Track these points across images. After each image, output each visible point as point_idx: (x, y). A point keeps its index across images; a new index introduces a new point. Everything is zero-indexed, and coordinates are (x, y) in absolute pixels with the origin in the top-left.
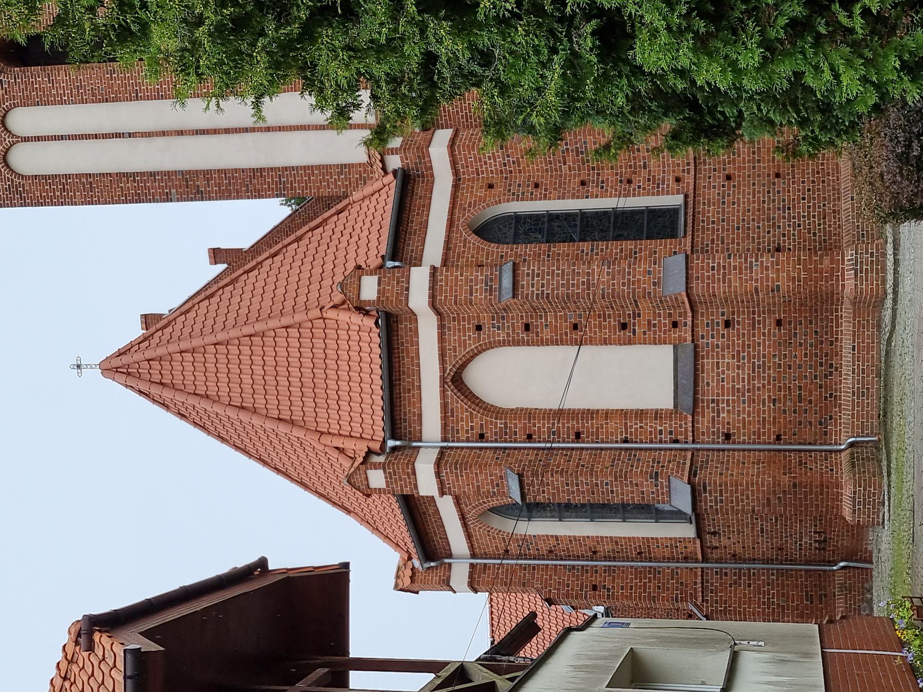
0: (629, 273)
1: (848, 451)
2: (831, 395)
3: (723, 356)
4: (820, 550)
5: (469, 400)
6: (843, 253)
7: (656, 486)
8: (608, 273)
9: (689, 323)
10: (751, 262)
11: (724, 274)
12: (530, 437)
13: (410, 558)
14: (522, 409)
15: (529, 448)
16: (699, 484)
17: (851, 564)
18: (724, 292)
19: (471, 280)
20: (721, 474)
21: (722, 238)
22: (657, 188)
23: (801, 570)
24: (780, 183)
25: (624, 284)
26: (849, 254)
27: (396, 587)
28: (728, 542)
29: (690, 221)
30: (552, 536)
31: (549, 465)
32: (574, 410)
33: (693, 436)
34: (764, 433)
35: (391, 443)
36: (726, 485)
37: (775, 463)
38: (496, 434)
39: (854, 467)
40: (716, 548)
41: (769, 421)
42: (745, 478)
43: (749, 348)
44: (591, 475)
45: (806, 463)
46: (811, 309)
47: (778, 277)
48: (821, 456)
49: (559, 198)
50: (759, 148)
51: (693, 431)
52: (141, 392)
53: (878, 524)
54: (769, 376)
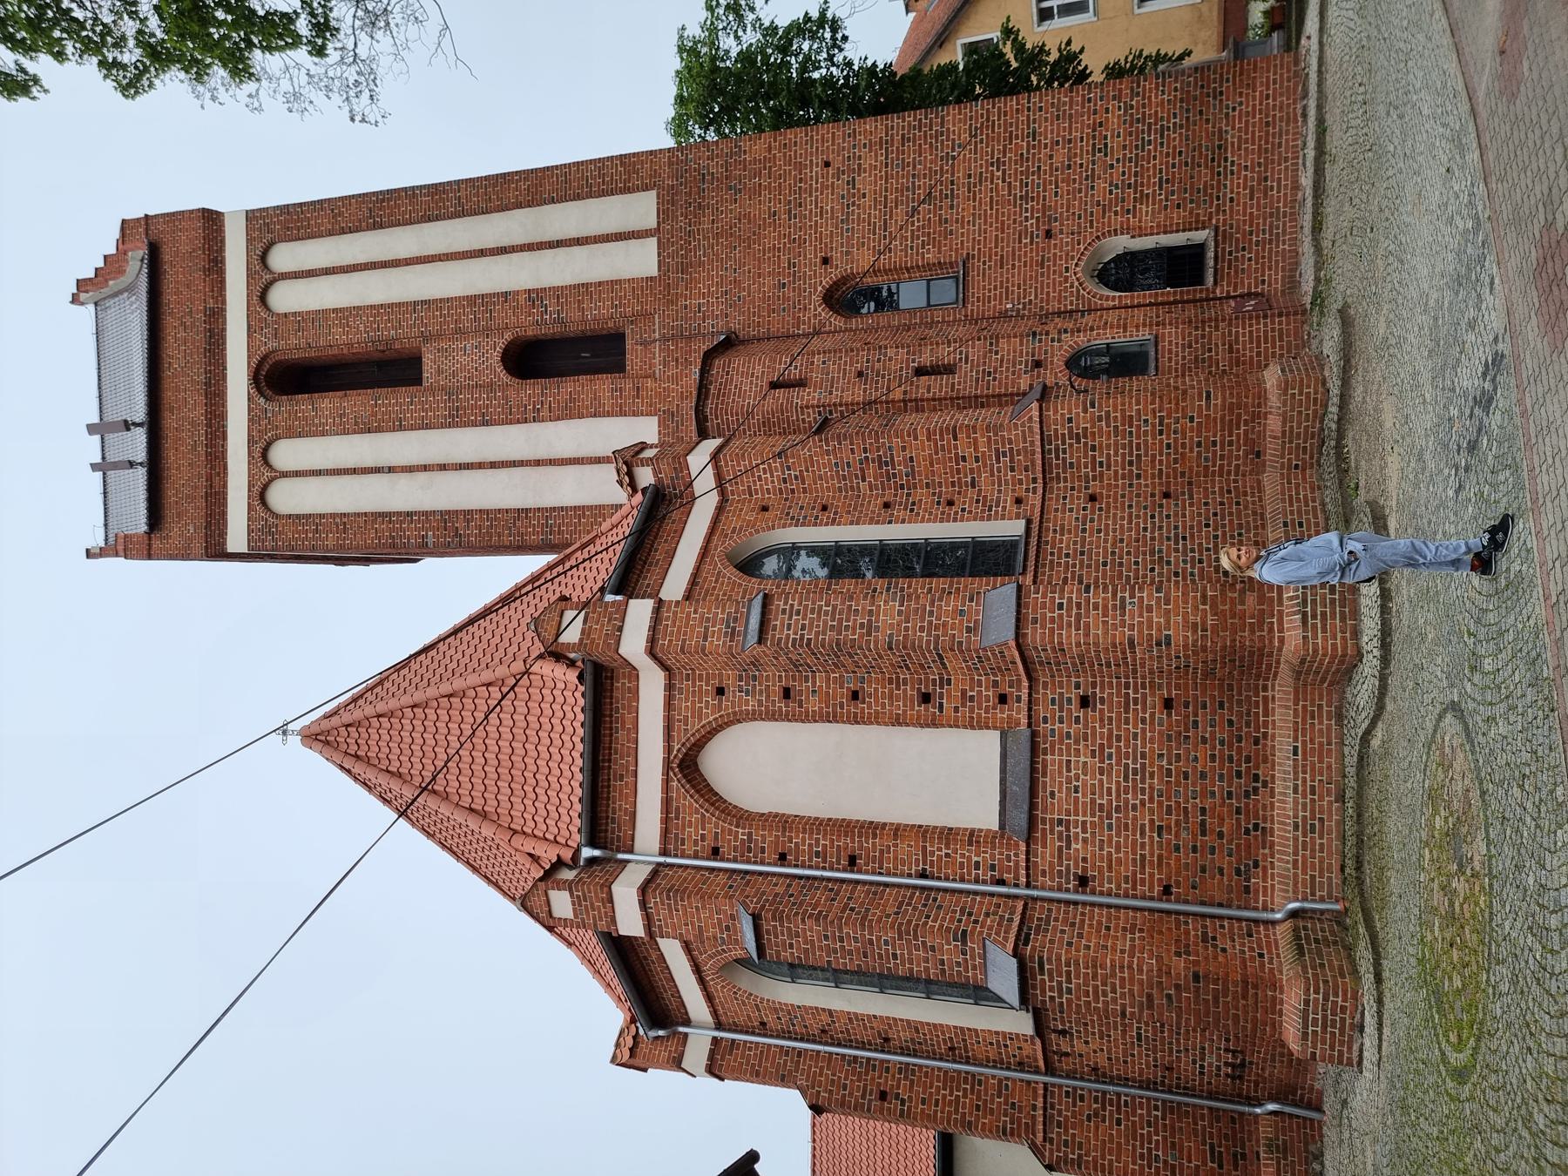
0: (931, 612)
1: (1288, 924)
2: (1256, 827)
4: (1233, 1078)
7: (965, 953)
9: (1025, 697)
10: (1123, 599)
11: (1078, 616)
12: (782, 859)
13: (633, 1021)
14: (776, 815)
15: (781, 875)
16: (1032, 957)
17: (1287, 1109)
18: (1078, 644)
20: (1070, 944)
21: (1081, 577)
22: (988, 511)
23: (1202, 1107)
24: (1170, 506)
25: (922, 629)
27: (613, 1060)
28: (1086, 1047)
32: (850, 822)
33: (1028, 876)
35: (587, 852)
36: (1077, 964)
37: (1160, 932)
38: (735, 849)
40: (1067, 1055)
41: (1152, 862)
42: (1111, 960)
44: (862, 925)
45: (1214, 938)
46: (1221, 686)
47: (1168, 622)
48: (1240, 928)
49: (852, 523)
51: (1028, 868)
52: (342, 768)
53: (1350, 1064)
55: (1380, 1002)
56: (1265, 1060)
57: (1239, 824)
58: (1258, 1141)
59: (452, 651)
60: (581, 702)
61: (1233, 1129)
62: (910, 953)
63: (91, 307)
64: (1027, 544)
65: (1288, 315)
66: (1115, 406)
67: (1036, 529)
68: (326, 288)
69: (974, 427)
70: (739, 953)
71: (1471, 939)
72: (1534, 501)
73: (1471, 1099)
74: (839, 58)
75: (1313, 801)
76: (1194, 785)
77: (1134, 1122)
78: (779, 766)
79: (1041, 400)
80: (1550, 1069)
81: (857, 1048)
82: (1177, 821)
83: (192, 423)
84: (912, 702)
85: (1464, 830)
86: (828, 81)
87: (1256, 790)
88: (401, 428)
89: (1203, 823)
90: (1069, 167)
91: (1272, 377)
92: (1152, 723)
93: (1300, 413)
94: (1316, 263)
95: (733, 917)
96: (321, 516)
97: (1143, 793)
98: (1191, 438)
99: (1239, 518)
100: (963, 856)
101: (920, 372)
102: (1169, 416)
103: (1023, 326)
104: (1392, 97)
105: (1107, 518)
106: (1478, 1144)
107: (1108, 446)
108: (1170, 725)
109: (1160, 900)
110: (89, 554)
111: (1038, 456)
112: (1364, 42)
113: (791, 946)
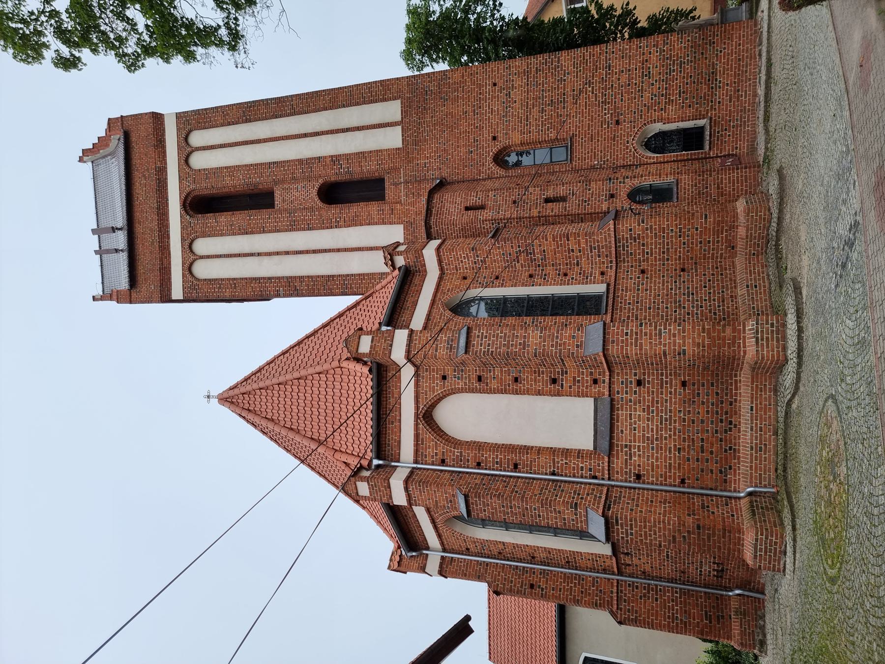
0: (557, 337)
1: (747, 499)
2: (730, 448)
3: (635, 409)
4: (717, 577)
6: (744, 324)
7: (576, 515)
8: (540, 337)
9: (607, 381)
10: (660, 330)
11: (636, 339)
12: (479, 465)
13: (399, 547)
14: (475, 442)
15: (478, 474)
16: (612, 517)
17: (746, 593)
18: (636, 354)
20: (632, 510)
21: (637, 315)
22: (586, 279)
23: (701, 592)
26: (751, 325)
27: (389, 568)
28: (641, 561)
29: (610, 302)
31: (490, 488)
32: (514, 446)
33: (609, 474)
34: (670, 476)
35: (376, 462)
36: (636, 520)
37: (679, 504)
38: (454, 460)
39: (754, 515)
40: (629, 565)
41: (675, 467)
42: (654, 520)
43: (657, 403)
45: (708, 507)
46: (712, 374)
47: (684, 342)
48: (722, 501)
50: (668, 249)
51: (609, 470)
52: (240, 415)
53: (779, 571)
54: (675, 428)
55: (795, 540)
56: (734, 568)
57: (721, 447)
58: (730, 609)
59: (298, 354)
60: (371, 383)
62: (547, 515)
63: (90, 164)
64: (607, 297)
65: (750, 167)
66: (655, 222)
67: (613, 288)
68: (222, 155)
70: (456, 513)
71: (839, 515)
72: (872, 304)
73: (838, 592)
74: (497, 15)
75: (761, 435)
76: (698, 426)
78: (473, 417)
79: (615, 220)
80: (872, 581)
82: (689, 445)
83: (151, 230)
85: (836, 460)
86: (492, 30)
87: (730, 429)
88: (264, 232)
89: (702, 446)
90: (629, 85)
91: (741, 205)
93: (756, 226)
94: (766, 139)
96: (222, 280)
100: (574, 464)
101: (547, 200)
103: (604, 174)
104: (807, 61)
105: (651, 283)
106: (840, 615)
107: (651, 244)
108: (685, 395)
110: (94, 299)
111: (613, 249)
112: (793, 22)
113: (485, 511)
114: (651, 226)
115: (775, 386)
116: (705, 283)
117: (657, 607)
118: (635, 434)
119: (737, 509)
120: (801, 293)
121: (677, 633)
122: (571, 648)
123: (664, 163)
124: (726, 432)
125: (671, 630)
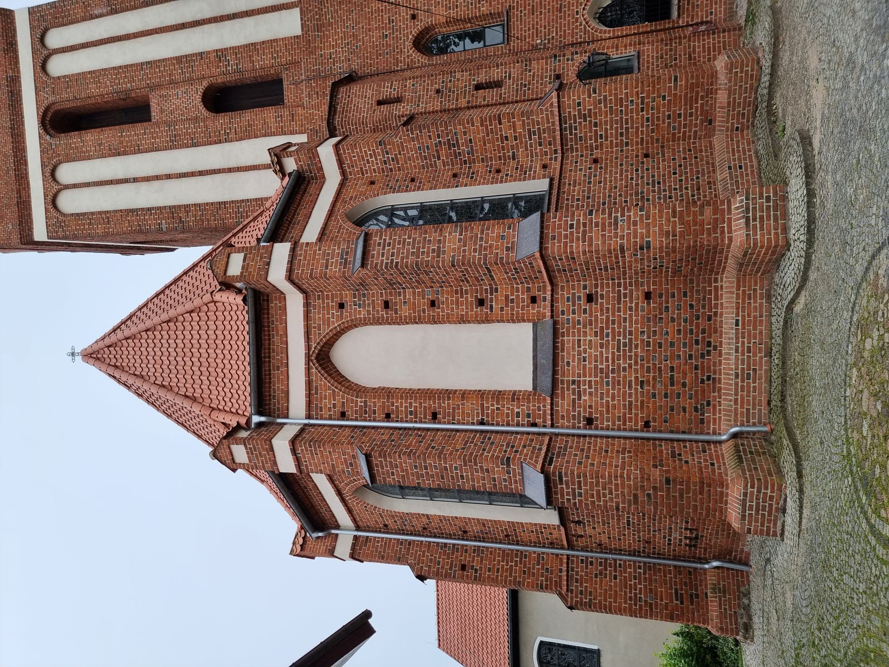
0: (482, 238)
1: (731, 442)
2: (709, 378)
3: (585, 332)
4: (690, 546)
5: (333, 378)
8: (460, 240)
9: (549, 298)
10: (616, 217)
11: (584, 232)
12: (388, 417)
13: (302, 528)
14: (384, 388)
15: (387, 428)
16: (554, 473)
18: (584, 253)
19: (328, 254)
20: (580, 463)
22: (524, 174)
23: (669, 566)
27: (291, 554)
28: (594, 531)
30: (423, 515)
32: (433, 390)
33: (552, 420)
34: (630, 419)
35: (256, 419)
37: (643, 452)
40: (581, 536)
41: (636, 406)
42: (609, 474)
45: (680, 455)
46: (685, 281)
47: (648, 232)
48: (698, 447)
49: (431, 189)
50: (627, 128)
51: (552, 415)
52: (110, 375)
53: (775, 534)
56: (711, 534)
61: (690, 578)
62: (472, 475)
65: (729, 31)
66: (610, 91)
67: (557, 185)
69: (513, 114)
75: (749, 357)
76: (666, 351)
77: (625, 577)
78: (378, 356)
81: (447, 538)
84: (472, 305)
87: (709, 353)
92: (637, 310)
93: (741, 86)
95: (354, 457)
96: (92, 213)
97: (630, 359)
98: (664, 112)
99: (697, 167)
100: (508, 409)
101: (478, 87)
102: (648, 97)
105: (606, 173)
107: (606, 122)
109: (642, 431)
113: (393, 474)
114: (605, 97)
115: (769, 291)
116: (675, 169)
117: (616, 586)
118: (585, 366)
119: (717, 456)
120: (811, 144)
121: (641, 617)
122: (526, 632)
123: (622, 37)
124: (703, 356)
125: (633, 614)
